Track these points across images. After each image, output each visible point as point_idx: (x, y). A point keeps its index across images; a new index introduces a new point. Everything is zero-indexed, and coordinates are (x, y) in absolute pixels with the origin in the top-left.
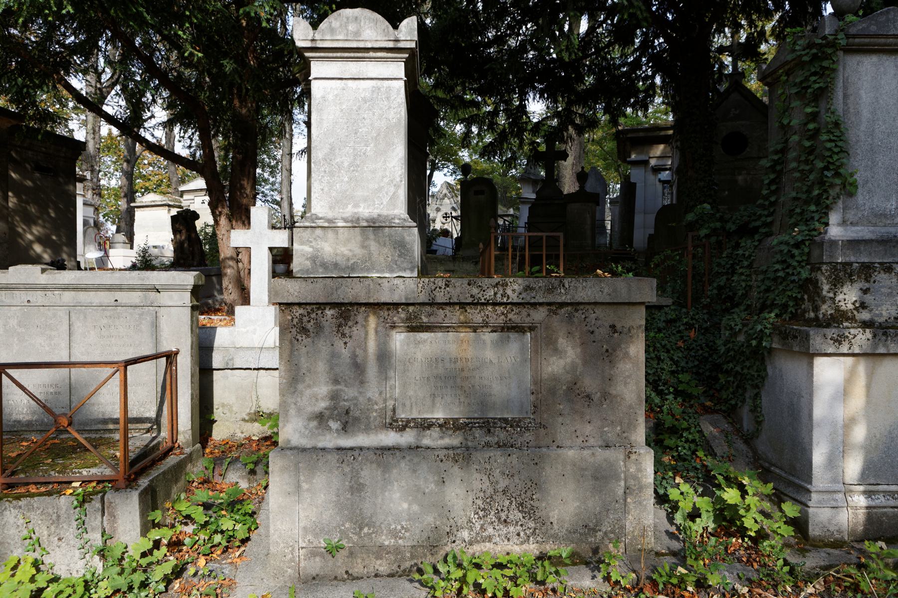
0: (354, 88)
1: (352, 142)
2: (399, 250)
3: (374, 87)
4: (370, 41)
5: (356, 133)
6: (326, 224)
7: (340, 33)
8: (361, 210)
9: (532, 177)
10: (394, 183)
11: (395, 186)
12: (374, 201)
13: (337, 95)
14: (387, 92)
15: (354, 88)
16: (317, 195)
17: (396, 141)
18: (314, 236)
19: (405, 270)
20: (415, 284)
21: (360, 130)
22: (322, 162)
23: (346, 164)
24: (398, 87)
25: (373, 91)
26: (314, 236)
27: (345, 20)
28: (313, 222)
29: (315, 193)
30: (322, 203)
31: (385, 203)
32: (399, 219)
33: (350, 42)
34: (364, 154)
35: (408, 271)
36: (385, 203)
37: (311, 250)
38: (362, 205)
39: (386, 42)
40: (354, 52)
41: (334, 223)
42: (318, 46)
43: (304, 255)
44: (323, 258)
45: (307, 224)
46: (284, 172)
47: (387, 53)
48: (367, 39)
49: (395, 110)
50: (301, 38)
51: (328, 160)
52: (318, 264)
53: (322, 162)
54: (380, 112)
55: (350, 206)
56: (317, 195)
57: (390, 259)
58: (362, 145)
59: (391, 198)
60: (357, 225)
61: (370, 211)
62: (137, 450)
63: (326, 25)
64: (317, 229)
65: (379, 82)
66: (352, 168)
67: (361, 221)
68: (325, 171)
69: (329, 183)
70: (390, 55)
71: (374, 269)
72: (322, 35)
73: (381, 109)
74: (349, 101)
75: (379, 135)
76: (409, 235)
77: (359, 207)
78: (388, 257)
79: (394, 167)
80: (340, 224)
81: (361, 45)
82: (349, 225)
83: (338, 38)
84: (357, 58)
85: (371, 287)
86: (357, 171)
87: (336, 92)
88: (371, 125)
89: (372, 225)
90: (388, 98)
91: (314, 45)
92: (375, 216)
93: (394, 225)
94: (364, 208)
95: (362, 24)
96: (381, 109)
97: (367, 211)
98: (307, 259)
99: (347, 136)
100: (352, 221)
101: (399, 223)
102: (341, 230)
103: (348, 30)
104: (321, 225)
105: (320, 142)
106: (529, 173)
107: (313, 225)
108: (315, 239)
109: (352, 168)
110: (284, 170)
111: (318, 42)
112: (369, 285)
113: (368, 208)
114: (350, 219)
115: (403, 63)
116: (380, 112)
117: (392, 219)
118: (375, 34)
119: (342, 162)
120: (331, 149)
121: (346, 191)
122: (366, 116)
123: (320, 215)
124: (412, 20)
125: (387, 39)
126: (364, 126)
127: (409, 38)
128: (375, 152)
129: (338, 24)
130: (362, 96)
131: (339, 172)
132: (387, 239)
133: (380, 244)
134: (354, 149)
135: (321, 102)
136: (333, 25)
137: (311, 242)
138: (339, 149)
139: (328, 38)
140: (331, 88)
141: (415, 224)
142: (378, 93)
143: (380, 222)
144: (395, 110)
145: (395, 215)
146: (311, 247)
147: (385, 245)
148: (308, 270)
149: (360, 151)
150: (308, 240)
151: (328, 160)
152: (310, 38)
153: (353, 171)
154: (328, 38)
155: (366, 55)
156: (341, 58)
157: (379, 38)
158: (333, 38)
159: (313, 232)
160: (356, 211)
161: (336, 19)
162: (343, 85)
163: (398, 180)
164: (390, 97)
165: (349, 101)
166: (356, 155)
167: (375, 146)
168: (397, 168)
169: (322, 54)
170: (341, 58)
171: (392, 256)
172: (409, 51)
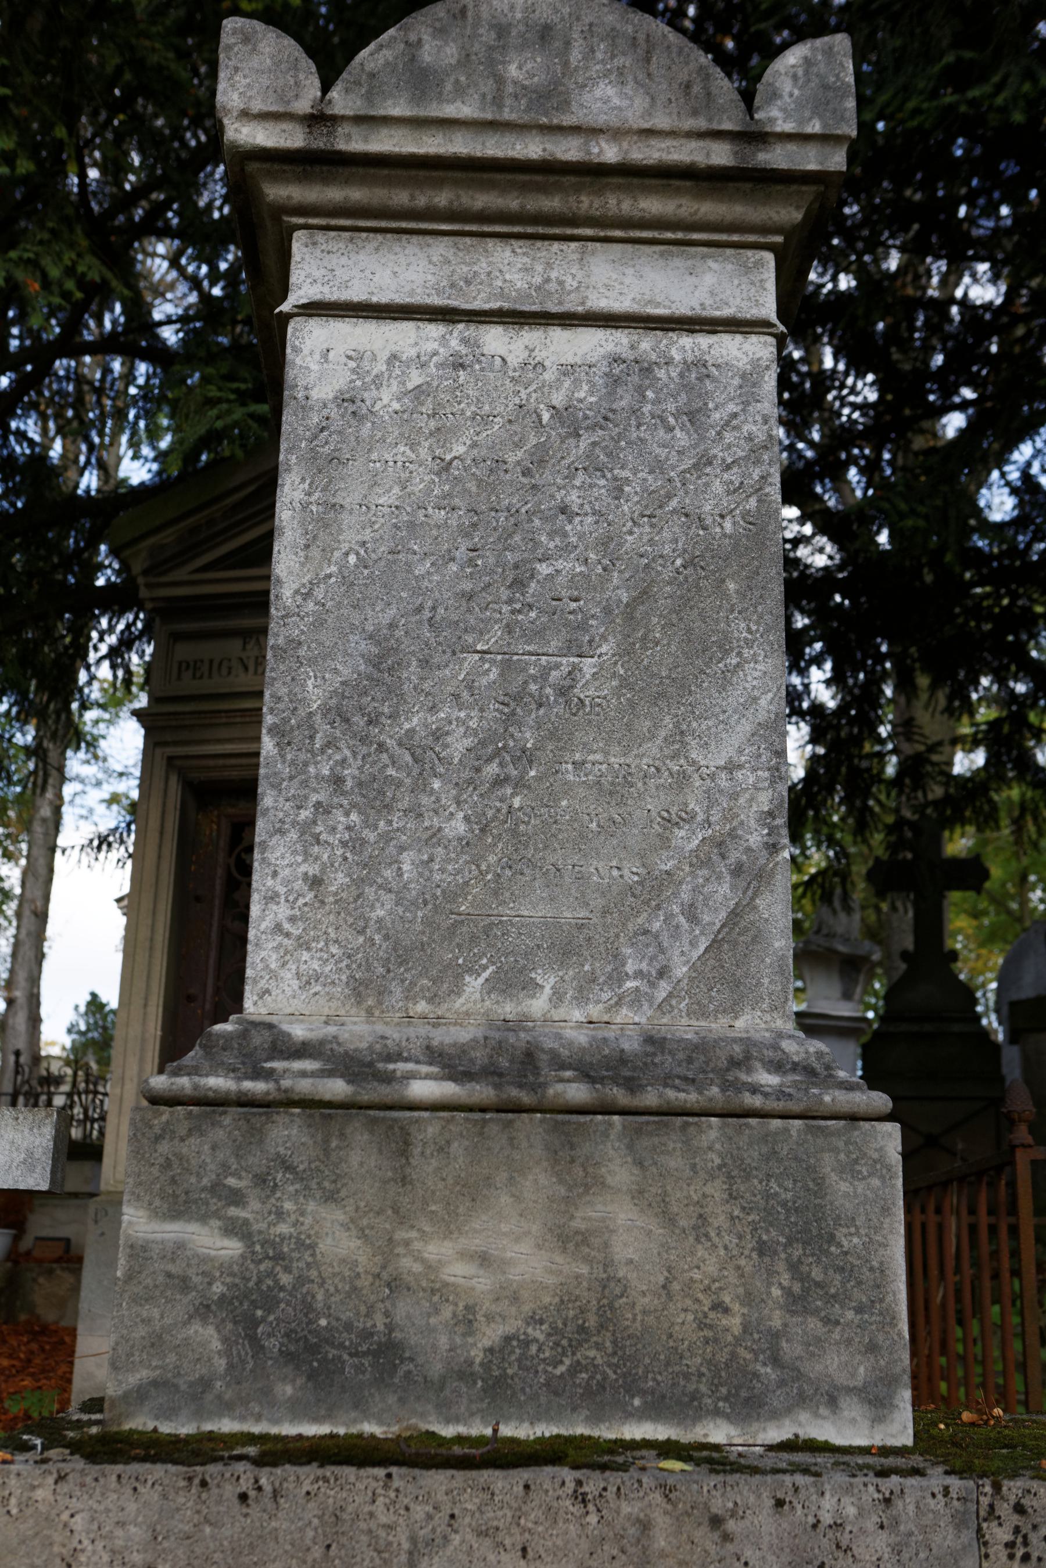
0: (513, 361)
1: (497, 631)
2: (794, 1267)
3: (617, 359)
4: (616, 133)
5: (518, 584)
6: (337, 1088)
7: (460, 92)
8: (538, 1005)
9: (841, 948)
10: (735, 855)
11: (737, 871)
12: (618, 958)
13: (419, 393)
14: (688, 388)
15: (513, 361)
16: (281, 911)
17: (740, 629)
18: (256, 1160)
19: (833, 1402)
20: (959, 1522)
21: (544, 569)
22: (323, 730)
23: (458, 745)
24: (743, 363)
25: (615, 382)
26: (256, 1160)
27: (488, 36)
28: (258, 1074)
29: (272, 898)
30: (310, 961)
31: (680, 971)
32: (777, 1066)
33: (509, 138)
34: (563, 692)
35: (852, 1408)
36: (680, 971)
37: (231, 1248)
38: (548, 982)
39: (694, 144)
40: (524, 188)
41: (388, 1078)
42: (342, 146)
43: (184, 1284)
44: (308, 1307)
45: (218, 1083)
46: (25, 921)
47: (700, 195)
48: (601, 120)
49: (734, 476)
50: (257, 106)
51: (359, 721)
52: (273, 1344)
53: (323, 730)
54: (654, 482)
55: (474, 984)
56: (281, 911)
57: (734, 1323)
58: (554, 645)
59: (715, 945)
60: (526, 1098)
61: (595, 1011)
62: (519, 251)
63: (387, 54)
64: (281, 1118)
65: (647, 343)
66: (492, 769)
67: (547, 1072)
68: (337, 781)
69: (355, 843)
70: (709, 209)
71: (631, 1386)
72: (369, 97)
73: (658, 467)
74: (486, 420)
75: (644, 595)
76: (849, 1170)
77: (532, 987)
78: (719, 1307)
79: (731, 767)
80: (422, 1089)
81: (569, 150)
82: (482, 1092)
83: (450, 110)
84: (538, 219)
85: (661, 1541)
86: (520, 784)
87: (416, 378)
88: (605, 542)
89: (620, 1096)
90: (694, 416)
91: (320, 144)
92: (631, 1045)
93: (756, 1102)
94: (557, 997)
95: (575, 56)
96: (658, 467)
97: (577, 1015)
98: (203, 1311)
99: (470, 597)
100: (490, 1073)
101: (780, 1094)
102: (432, 1127)
103: (500, 81)
104: (305, 1087)
105: (319, 623)
106: (832, 935)
107: (257, 1087)
108: (261, 1180)
109: (492, 769)
110: (27, 913)
111: (342, 130)
112: (645, 1526)
113: (581, 998)
114: (480, 1056)
115: (769, 257)
116: (654, 482)
117: (735, 1063)
118: (640, 103)
119: (438, 735)
120: (376, 663)
121: (452, 895)
122: (574, 498)
123: (299, 1032)
124: (829, 52)
125: (701, 123)
126: (567, 549)
127: (815, 127)
128: (625, 683)
129: (451, 53)
130: (558, 399)
131: (420, 786)
132: (716, 1189)
133: (670, 1220)
134: (507, 667)
135: (337, 424)
136: (427, 54)
137: (237, 1198)
138: (425, 663)
139: (398, 109)
140: (394, 357)
141: (880, 1101)
142: (641, 391)
143: (667, 1081)
144: (734, 476)
145: (748, 1043)
146: (233, 1229)
147: (701, 1228)
148: (205, 1383)
149: (545, 672)
150: (216, 1188)
151: (359, 721)
152: (303, 106)
153: (499, 782)
154: (396, 112)
155: (586, 203)
156: (451, 216)
157: (662, 121)
158: (422, 113)
159: (256, 1135)
160: (508, 1009)
161: (441, 32)
162: (454, 343)
163: (755, 839)
164: (704, 410)
165: (486, 420)
166: (518, 698)
167: (625, 652)
168: (746, 777)
169: (357, 195)
170: (451, 216)
171: (748, 1299)
172: (810, 190)
